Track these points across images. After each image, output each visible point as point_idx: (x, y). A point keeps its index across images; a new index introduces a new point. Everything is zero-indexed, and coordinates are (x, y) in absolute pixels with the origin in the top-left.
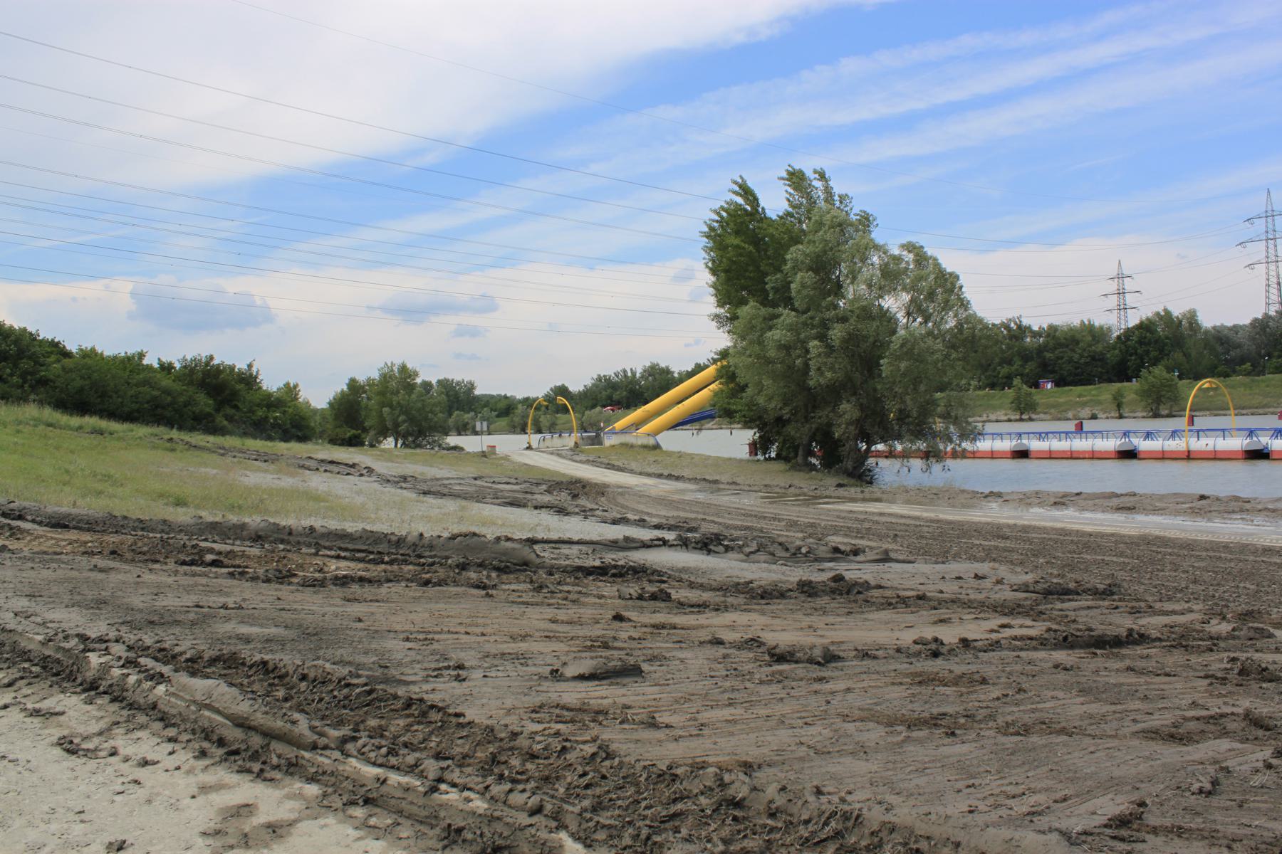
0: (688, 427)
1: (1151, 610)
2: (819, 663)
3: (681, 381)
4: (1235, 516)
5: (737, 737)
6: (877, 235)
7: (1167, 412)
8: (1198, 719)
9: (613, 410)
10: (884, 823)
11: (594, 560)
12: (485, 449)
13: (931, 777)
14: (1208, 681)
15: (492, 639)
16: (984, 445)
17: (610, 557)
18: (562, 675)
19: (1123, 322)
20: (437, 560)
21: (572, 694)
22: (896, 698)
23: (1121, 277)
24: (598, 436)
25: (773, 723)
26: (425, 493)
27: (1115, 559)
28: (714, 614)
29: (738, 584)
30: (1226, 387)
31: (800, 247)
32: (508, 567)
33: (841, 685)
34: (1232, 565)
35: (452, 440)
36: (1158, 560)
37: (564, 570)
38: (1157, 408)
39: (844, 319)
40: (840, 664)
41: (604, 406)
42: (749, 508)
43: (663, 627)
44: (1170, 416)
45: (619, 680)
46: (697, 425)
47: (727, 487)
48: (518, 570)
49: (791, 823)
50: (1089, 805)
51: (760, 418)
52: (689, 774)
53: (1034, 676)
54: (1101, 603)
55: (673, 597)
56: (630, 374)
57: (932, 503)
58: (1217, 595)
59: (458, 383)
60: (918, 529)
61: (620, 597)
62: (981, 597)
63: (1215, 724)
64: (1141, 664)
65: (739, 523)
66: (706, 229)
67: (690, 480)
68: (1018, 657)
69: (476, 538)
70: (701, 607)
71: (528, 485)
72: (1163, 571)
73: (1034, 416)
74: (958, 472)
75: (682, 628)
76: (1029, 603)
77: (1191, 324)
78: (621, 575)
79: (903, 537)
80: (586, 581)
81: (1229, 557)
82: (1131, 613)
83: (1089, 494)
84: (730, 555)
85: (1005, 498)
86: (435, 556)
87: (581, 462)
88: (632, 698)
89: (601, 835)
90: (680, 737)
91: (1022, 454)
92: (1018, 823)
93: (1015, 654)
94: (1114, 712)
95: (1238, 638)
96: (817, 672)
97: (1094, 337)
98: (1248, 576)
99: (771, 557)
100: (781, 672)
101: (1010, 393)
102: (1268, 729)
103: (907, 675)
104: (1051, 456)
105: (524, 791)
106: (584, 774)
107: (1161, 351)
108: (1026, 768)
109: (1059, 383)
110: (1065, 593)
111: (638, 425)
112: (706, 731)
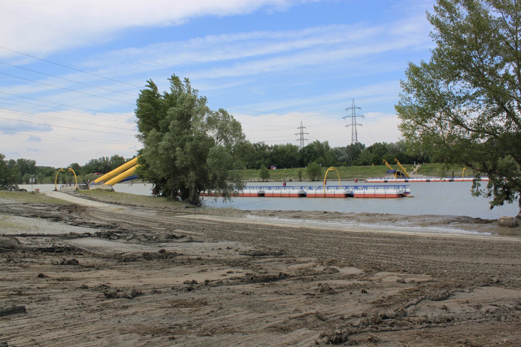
0: (128, 182)
1: (296, 262)
2: (129, 298)
4: (335, 220)
8: (296, 318)
9: (98, 174)
12: (34, 190)
16: (246, 191)
17: (58, 243)
19: (302, 145)
23: (302, 128)
24: (87, 185)
27: (289, 238)
29: (116, 255)
30: (338, 170)
31: (174, 108)
34: (332, 239)
35: (21, 187)
36: (306, 238)
38: (314, 178)
40: (141, 297)
41: (94, 173)
42: (146, 217)
44: (318, 181)
47: (139, 208)
54: (276, 259)
55: (80, 262)
56: (106, 159)
57: (222, 215)
58: (324, 253)
59: (28, 161)
61: (52, 264)
63: (302, 320)
64: (282, 289)
65: (139, 224)
67: (124, 205)
68: (229, 289)
70: (90, 267)
71: (49, 207)
72: (306, 243)
73: (268, 180)
74: (236, 202)
75: (73, 280)
76: (246, 260)
77: (326, 146)
79: (206, 229)
81: (332, 236)
83: (284, 211)
84: (120, 240)
85: (252, 213)
87: (78, 196)
91: (262, 195)
94: (260, 317)
95: (325, 273)
98: (336, 244)
99: (138, 241)
100: (106, 304)
101: (260, 171)
104: (273, 196)
107: (316, 156)
109: (278, 167)
110: (262, 255)
111: (105, 181)
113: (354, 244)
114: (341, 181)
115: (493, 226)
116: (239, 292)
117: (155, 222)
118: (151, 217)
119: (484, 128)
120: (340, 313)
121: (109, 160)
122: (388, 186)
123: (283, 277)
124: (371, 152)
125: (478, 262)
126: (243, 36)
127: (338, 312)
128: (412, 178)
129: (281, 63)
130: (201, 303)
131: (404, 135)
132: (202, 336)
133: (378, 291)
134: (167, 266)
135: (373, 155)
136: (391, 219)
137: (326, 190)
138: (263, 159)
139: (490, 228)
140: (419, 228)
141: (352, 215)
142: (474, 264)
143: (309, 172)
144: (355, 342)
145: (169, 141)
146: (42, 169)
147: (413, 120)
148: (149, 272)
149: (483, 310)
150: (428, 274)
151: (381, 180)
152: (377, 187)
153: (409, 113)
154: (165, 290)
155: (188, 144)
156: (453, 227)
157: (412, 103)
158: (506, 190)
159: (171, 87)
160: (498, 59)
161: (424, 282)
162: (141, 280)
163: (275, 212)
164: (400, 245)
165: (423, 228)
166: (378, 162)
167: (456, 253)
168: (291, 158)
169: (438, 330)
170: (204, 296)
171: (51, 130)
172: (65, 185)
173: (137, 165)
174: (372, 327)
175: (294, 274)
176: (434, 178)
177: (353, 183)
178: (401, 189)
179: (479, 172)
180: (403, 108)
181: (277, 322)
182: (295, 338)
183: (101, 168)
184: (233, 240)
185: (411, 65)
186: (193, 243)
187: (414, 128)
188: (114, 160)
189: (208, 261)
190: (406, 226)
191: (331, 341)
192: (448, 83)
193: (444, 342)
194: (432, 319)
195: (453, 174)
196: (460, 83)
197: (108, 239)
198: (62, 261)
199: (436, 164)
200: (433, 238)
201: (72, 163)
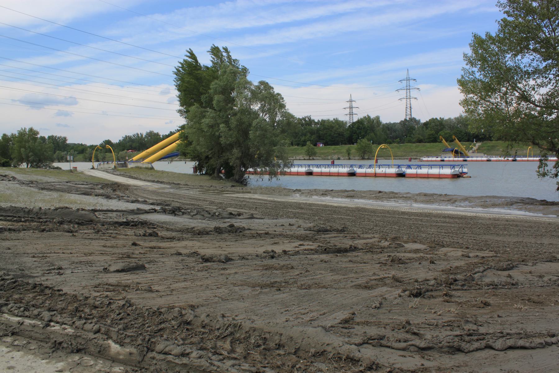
1: (359, 238)
2: (223, 262)
5: (188, 295)
10: (251, 328)
12: (72, 168)
13: (271, 308)
14: (380, 265)
15: (76, 255)
16: (294, 170)
17: (130, 217)
20: (48, 220)
21: (113, 279)
22: (256, 276)
23: (351, 101)
24: (125, 163)
26: (42, 189)
27: (346, 217)
28: (178, 242)
29: (188, 229)
32: (83, 222)
33: (233, 271)
34: (390, 219)
35: (56, 164)
37: (110, 224)
38: (364, 156)
42: (193, 196)
43: (155, 248)
44: (368, 159)
45: (135, 272)
47: (183, 186)
51: (198, 156)
52: (167, 311)
54: (340, 235)
56: (140, 136)
59: (59, 138)
60: (266, 205)
61: (135, 235)
62: (292, 233)
63: (382, 281)
64: (355, 259)
65: (189, 202)
68: (306, 257)
70: (172, 239)
73: (315, 158)
74: (283, 180)
75: (163, 248)
76: (311, 235)
78: (136, 225)
79: (259, 208)
80: (119, 228)
81: (389, 216)
84: (185, 216)
87: (117, 175)
88: (141, 279)
90: (163, 295)
91: (310, 174)
93: (305, 256)
94: (344, 278)
96: (222, 266)
100: (207, 266)
102: (400, 282)
103: (261, 266)
104: (321, 174)
105: (91, 323)
106: (120, 314)
107: (366, 132)
109: (326, 144)
110: (325, 231)
112: (174, 293)
113: (413, 224)
120: (413, 277)
123: (354, 249)
124: (427, 128)
125: (542, 242)
128: (472, 157)
129: (322, 29)
130: (287, 268)
133: (446, 263)
134: (240, 239)
135: (428, 132)
136: (450, 200)
138: (309, 135)
140: (480, 209)
141: (408, 195)
142: (537, 244)
143: (359, 150)
144: (433, 296)
147: (476, 95)
149: (546, 279)
152: (431, 166)
156: (516, 208)
159: (212, 59)
161: (489, 257)
163: (327, 191)
164: (461, 225)
165: (485, 209)
166: (434, 139)
176: (495, 157)
177: (407, 162)
178: (457, 169)
179: (545, 151)
185: (476, 36)
188: (149, 136)
189: (275, 236)
190: (466, 206)
191: (413, 295)
192: (516, 55)
193: (509, 299)
194: (498, 283)
195: (516, 153)
197: (173, 215)
198: (144, 232)
199: (498, 142)
200: (495, 219)
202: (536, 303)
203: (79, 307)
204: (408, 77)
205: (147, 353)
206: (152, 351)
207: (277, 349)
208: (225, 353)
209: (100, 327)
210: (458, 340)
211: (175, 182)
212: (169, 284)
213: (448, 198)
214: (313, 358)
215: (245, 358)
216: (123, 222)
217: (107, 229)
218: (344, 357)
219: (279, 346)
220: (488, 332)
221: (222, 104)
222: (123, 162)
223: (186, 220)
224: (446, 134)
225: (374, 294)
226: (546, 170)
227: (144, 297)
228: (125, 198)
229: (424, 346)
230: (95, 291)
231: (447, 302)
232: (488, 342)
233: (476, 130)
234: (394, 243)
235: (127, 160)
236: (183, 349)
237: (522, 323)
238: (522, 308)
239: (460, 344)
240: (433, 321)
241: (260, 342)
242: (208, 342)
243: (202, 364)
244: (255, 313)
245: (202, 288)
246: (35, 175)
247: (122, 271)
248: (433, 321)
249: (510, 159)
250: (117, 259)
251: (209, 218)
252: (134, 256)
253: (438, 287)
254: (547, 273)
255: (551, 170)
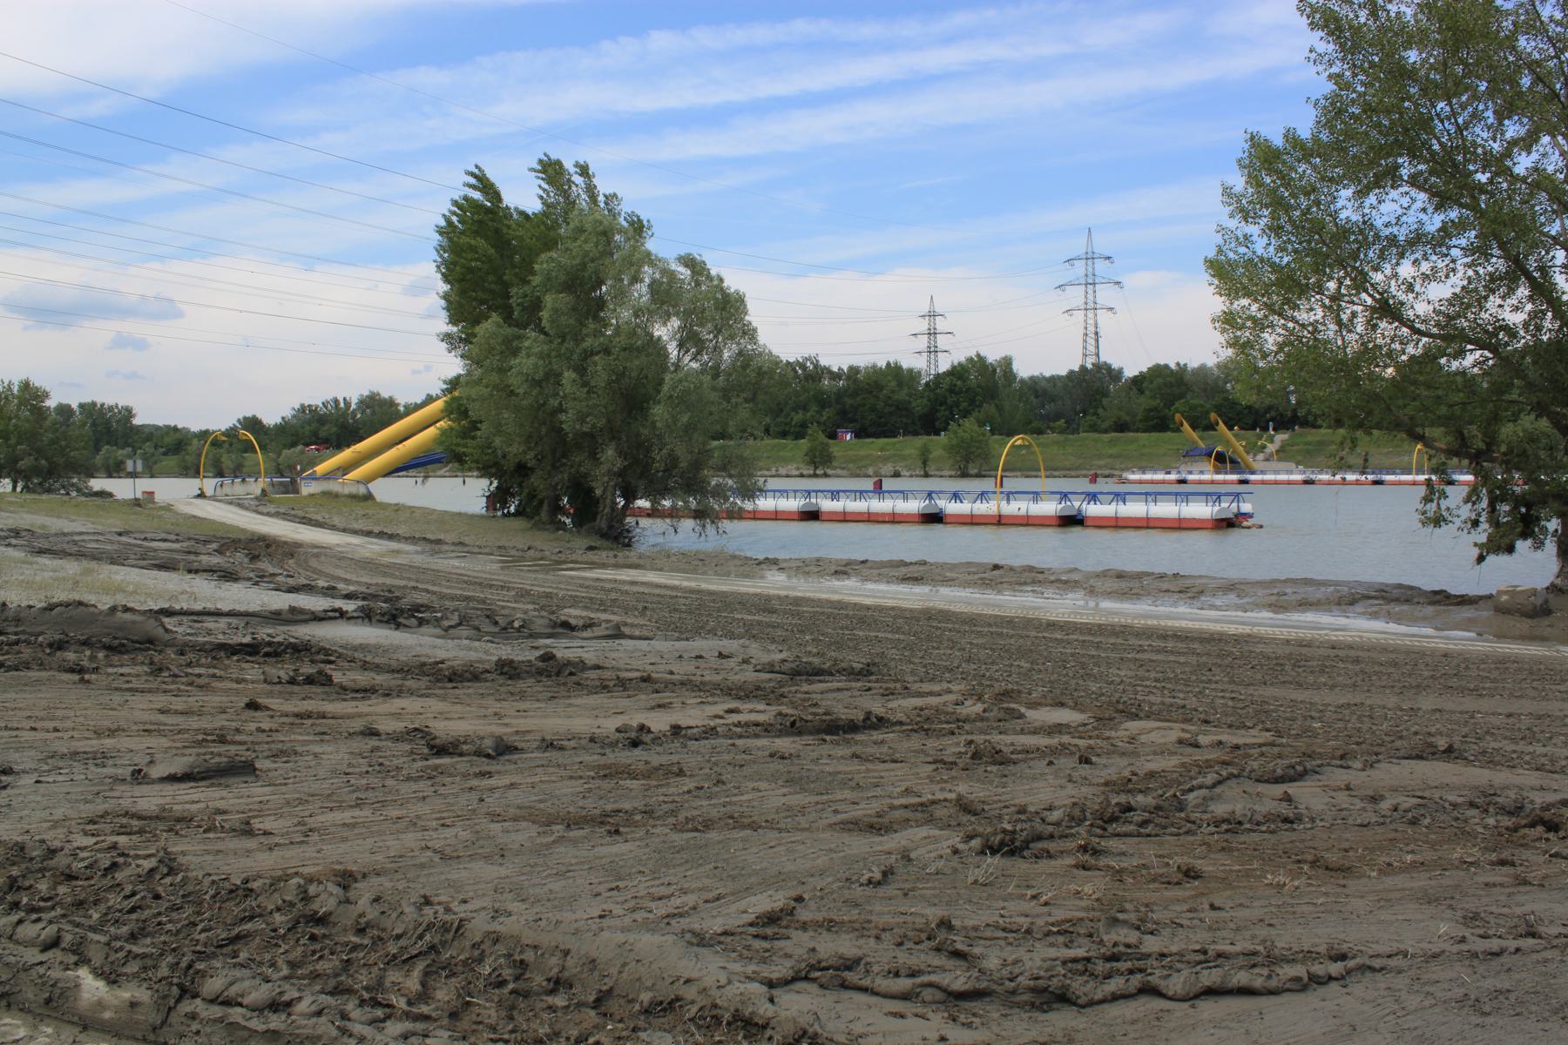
0: (412, 472)
1: (907, 691)
2: (488, 756)
3: (400, 417)
5: (350, 843)
6: (651, 245)
7: (976, 471)
10: (489, 933)
11: (244, 636)
12: (139, 495)
13: (571, 881)
14: (934, 766)
15: (66, 736)
16: (765, 504)
17: (265, 632)
18: (146, 775)
20: (23, 637)
21: (149, 799)
22: (567, 793)
23: (932, 315)
24: (293, 482)
25: (401, 825)
26: (41, 552)
27: (890, 636)
28: (381, 699)
29: (424, 664)
30: (1038, 445)
32: (123, 645)
33: (506, 781)
35: (97, 484)
37: (202, 649)
38: (966, 467)
39: (607, 351)
40: (516, 756)
41: (307, 445)
42: (475, 574)
43: (309, 716)
45: (223, 781)
46: (421, 472)
47: (453, 548)
48: (139, 649)
49: (381, 939)
50: (743, 904)
51: (496, 464)
52: (267, 887)
53: (742, 766)
56: (342, 405)
57: (694, 571)
59: (111, 409)
60: (674, 601)
61: (265, 681)
62: (718, 678)
63: (922, 811)
65: (459, 592)
66: (443, 223)
67: (406, 539)
68: (734, 745)
69: (82, 608)
70: (367, 692)
72: (938, 648)
73: (830, 472)
74: (737, 536)
75: (333, 718)
77: (1005, 372)
78: (276, 654)
79: (653, 609)
80: (226, 662)
82: (883, 695)
84: (424, 629)
85: (782, 565)
86: (23, 632)
87: (268, 514)
88: (231, 801)
89: (132, 968)
90: (277, 845)
91: (812, 515)
92: (652, 926)
93: (730, 741)
94: (817, 803)
96: (484, 765)
97: (900, 384)
100: (436, 768)
101: (804, 443)
102: (975, 814)
103: (592, 768)
104: (844, 518)
105: (38, 920)
106: (133, 894)
107: (972, 402)
108: (688, 866)
110: (817, 673)
111: (346, 469)
112: (315, 837)
113: (1072, 655)
114: (1047, 477)
115: (1476, 614)
116: (760, 753)
117: (502, 588)
118: (489, 573)
119: (1464, 329)
120: (1017, 801)
121: (353, 406)
122: (1188, 494)
124: (1141, 392)
126: (761, 33)
127: (1013, 799)
128: (1263, 472)
129: (878, 116)
131: (1230, 345)
132: (682, 831)
133: (1124, 762)
135: (1143, 403)
137: (1004, 503)
139: (1470, 620)
140: (1266, 614)
141: (1075, 577)
142: (1402, 710)
143: (951, 449)
144: (1048, 852)
145: (541, 356)
146: (151, 434)
147: (1256, 300)
148: (522, 705)
149: (1385, 806)
150: (1268, 730)
151: (1168, 477)
152: (1153, 496)
153: (1245, 280)
154: (572, 743)
155: (599, 363)
156: (1363, 613)
157: (1254, 252)
158: (1523, 510)
159: (541, 192)
160: (1513, 129)
161: (1252, 746)
162: (506, 721)
163: (849, 563)
164: (1204, 659)
166: (1160, 423)
167: (1360, 683)
168: (898, 408)
169: (1255, 837)
170: (675, 758)
171: (180, 315)
172: (227, 481)
173: (442, 423)
174: (1092, 825)
175: (904, 719)
177: (1083, 485)
180: (1230, 265)
181: (860, 813)
182: (903, 843)
183: (327, 430)
184: (732, 636)
186: (622, 641)
187: (1259, 325)
189: (670, 685)
190: (1227, 608)
192: (1361, 194)
194: (1245, 815)
196: (1396, 198)
198: (291, 674)
200: (1301, 643)
201: (241, 417)
202: (1332, 870)
203: (24, 876)
204: (1090, 250)
205: (178, 1001)
206: (195, 996)
207: (552, 992)
208: (401, 1003)
209: (59, 930)
210: (1063, 972)
211: (429, 536)
212: (307, 813)
213: (1182, 583)
214: (642, 1018)
215: (454, 1015)
216: (241, 644)
217: (189, 665)
218: (727, 1016)
219: (558, 984)
220: (1165, 951)
221: (568, 321)
222: (287, 478)
223: (427, 640)
224: (1193, 408)
225: (886, 847)
226: (1443, 507)
227: (221, 848)
228: (280, 579)
229: (963, 988)
230: (86, 834)
231: (1084, 868)
232: (1149, 978)
233: (1254, 398)
234: (996, 708)
235: (299, 474)
236: (278, 990)
237: (1270, 925)
238: (1285, 884)
239: (1068, 982)
240: (1022, 920)
241: (507, 973)
242: (364, 971)
243: (319, 1032)
244: (518, 895)
245: (398, 826)
246: (28, 512)
247: (186, 777)
248: (1022, 920)
249: (1350, 477)
250: (185, 747)
251: (493, 634)
252: (238, 738)
253: (1072, 827)
254: (1394, 790)
255: (1458, 507)
